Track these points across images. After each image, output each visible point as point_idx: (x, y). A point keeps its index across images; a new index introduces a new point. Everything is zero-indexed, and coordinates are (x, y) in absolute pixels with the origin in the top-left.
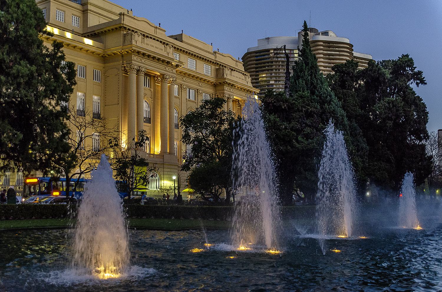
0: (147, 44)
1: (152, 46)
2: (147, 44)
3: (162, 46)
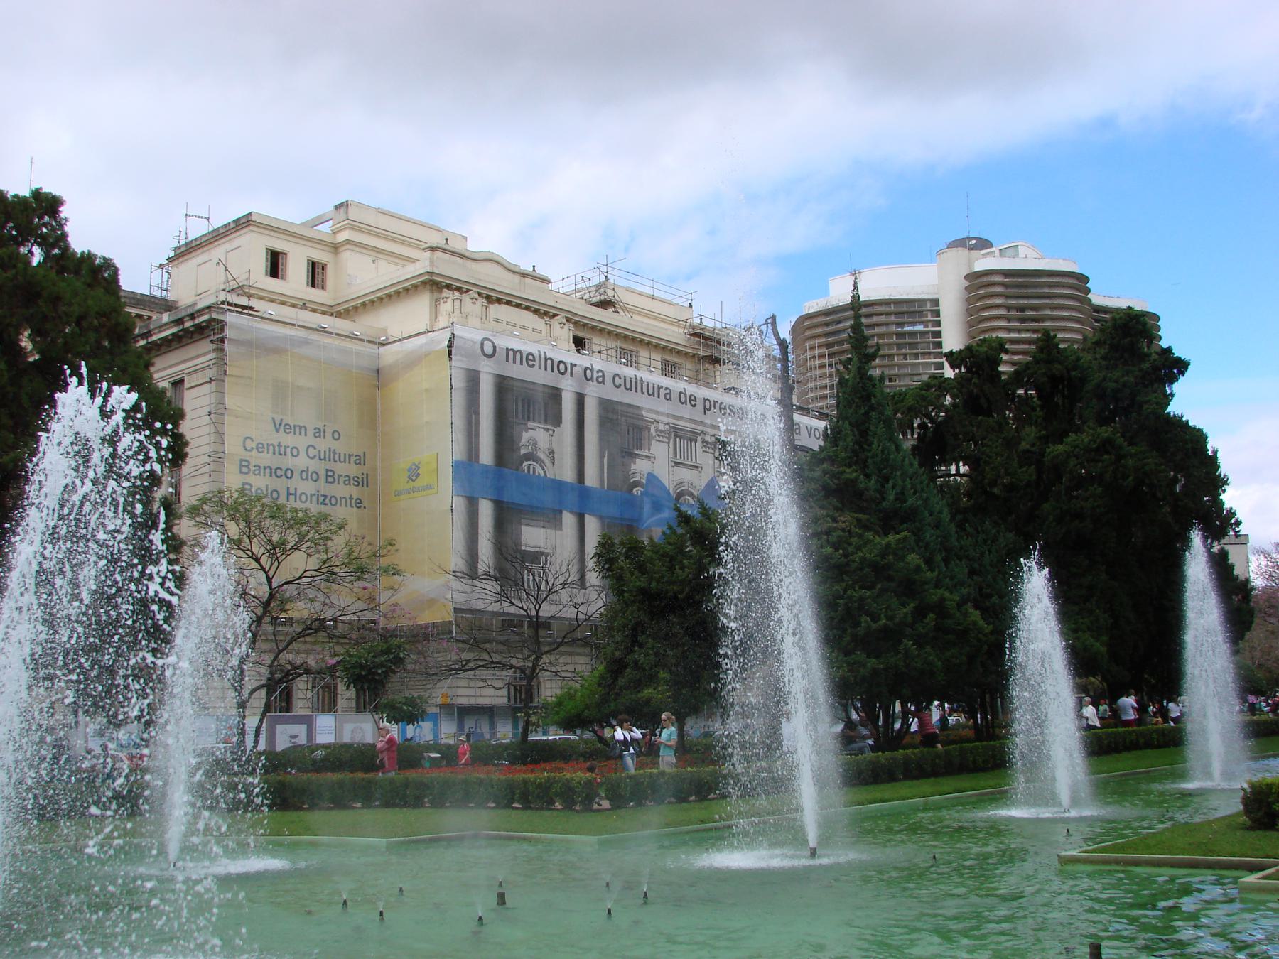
2: (497, 320)
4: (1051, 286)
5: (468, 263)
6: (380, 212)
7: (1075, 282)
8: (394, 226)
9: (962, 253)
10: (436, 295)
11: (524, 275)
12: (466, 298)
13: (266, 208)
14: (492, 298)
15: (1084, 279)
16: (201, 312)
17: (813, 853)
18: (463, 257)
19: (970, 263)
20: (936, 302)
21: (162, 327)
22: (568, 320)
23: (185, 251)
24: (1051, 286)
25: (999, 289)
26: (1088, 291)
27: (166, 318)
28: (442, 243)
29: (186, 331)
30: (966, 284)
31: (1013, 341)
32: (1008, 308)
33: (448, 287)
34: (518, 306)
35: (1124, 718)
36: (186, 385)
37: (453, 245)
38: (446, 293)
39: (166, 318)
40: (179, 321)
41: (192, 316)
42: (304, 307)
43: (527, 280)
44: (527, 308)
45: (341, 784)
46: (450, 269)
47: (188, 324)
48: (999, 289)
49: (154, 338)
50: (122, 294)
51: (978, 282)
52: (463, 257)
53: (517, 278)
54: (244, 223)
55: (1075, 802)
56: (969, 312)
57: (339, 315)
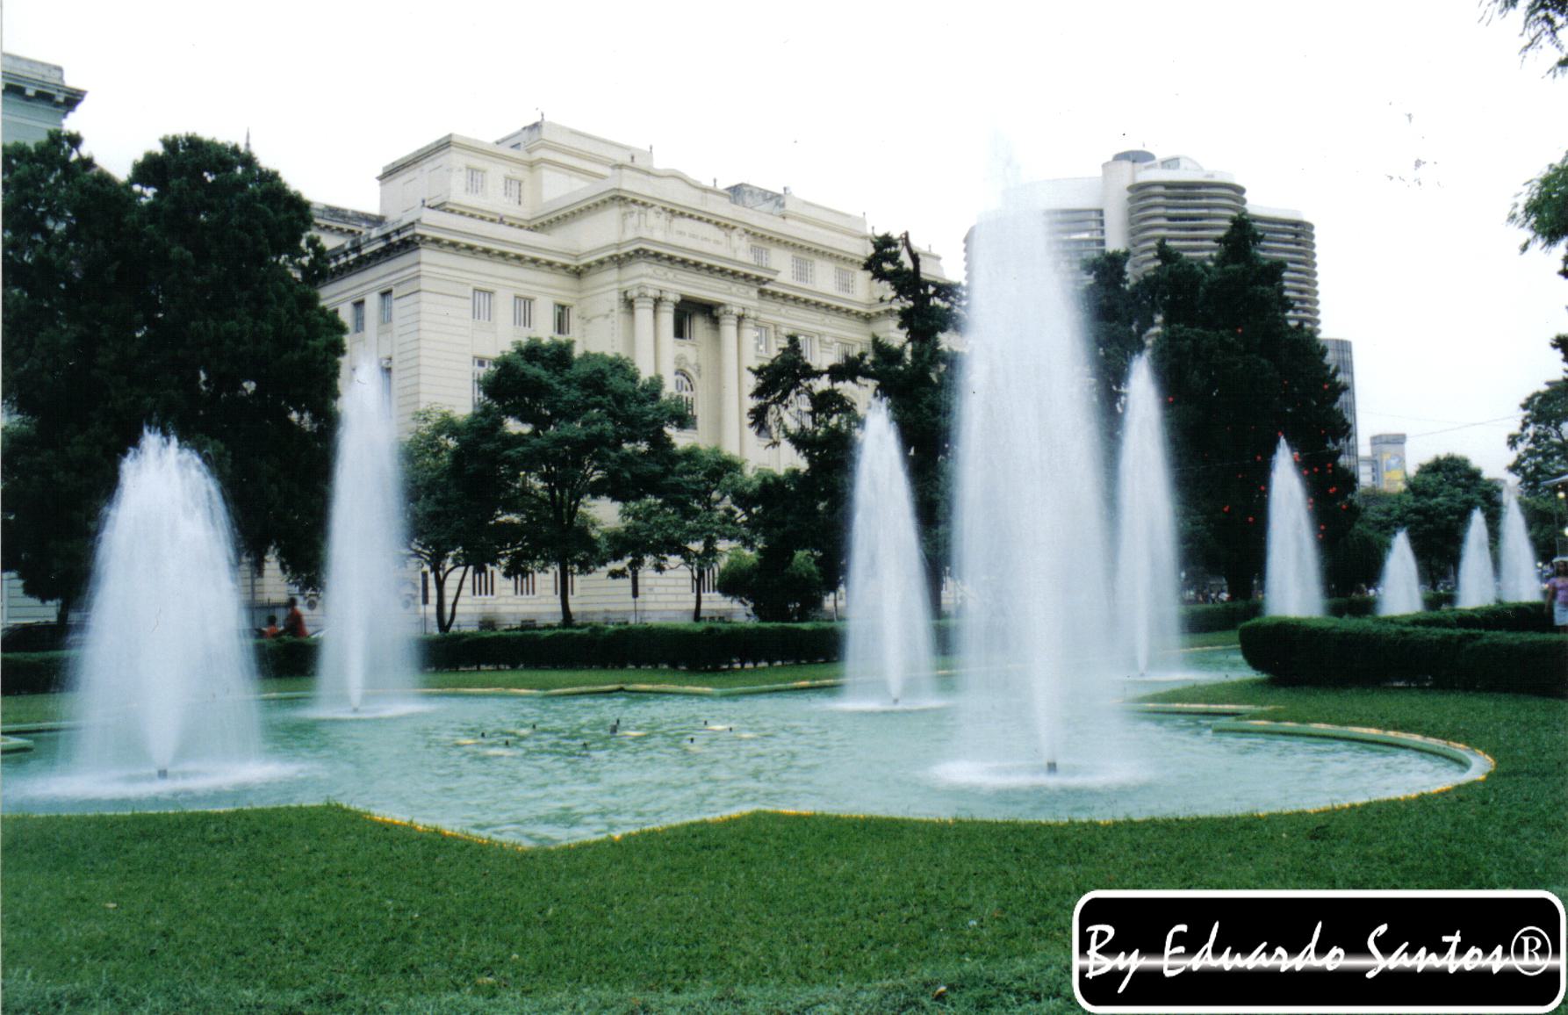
0: (681, 233)
1: (693, 236)
2: (681, 233)
3: (718, 234)
4: (1210, 196)
5: (652, 179)
6: (573, 132)
7: (1232, 193)
8: (587, 147)
9: (1126, 165)
10: (624, 210)
11: (705, 190)
12: (651, 212)
13: (464, 130)
14: (674, 213)
15: (1240, 190)
16: (405, 228)
17: (896, 701)
18: (648, 173)
19: (1134, 175)
20: (1101, 212)
21: (369, 241)
22: (747, 232)
23: (390, 173)
24: (1210, 196)
25: (1160, 200)
26: (1244, 201)
27: (375, 233)
28: (627, 160)
29: (392, 245)
30: (1128, 194)
31: (1293, 262)
32: (1171, 219)
33: (634, 202)
34: (700, 219)
35: (53, 619)
36: (395, 294)
37: (639, 163)
38: (635, 208)
39: (375, 233)
40: (386, 237)
41: (398, 232)
42: (501, 221)
43: (710, 196)
44: (708, 221)
45: (801, 620)
46: (631, 184)
47: (395, 239)
48: (1160, 200)
49: (364, 252)
50: (313, 212)
51: (1140, 191)
52: (648, 173)
53: (698, 193)
54: (445, 145)
55: (1152, 664)
56: (1131, 222)
57: (534, 229)
